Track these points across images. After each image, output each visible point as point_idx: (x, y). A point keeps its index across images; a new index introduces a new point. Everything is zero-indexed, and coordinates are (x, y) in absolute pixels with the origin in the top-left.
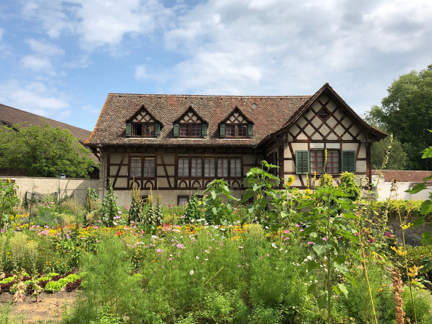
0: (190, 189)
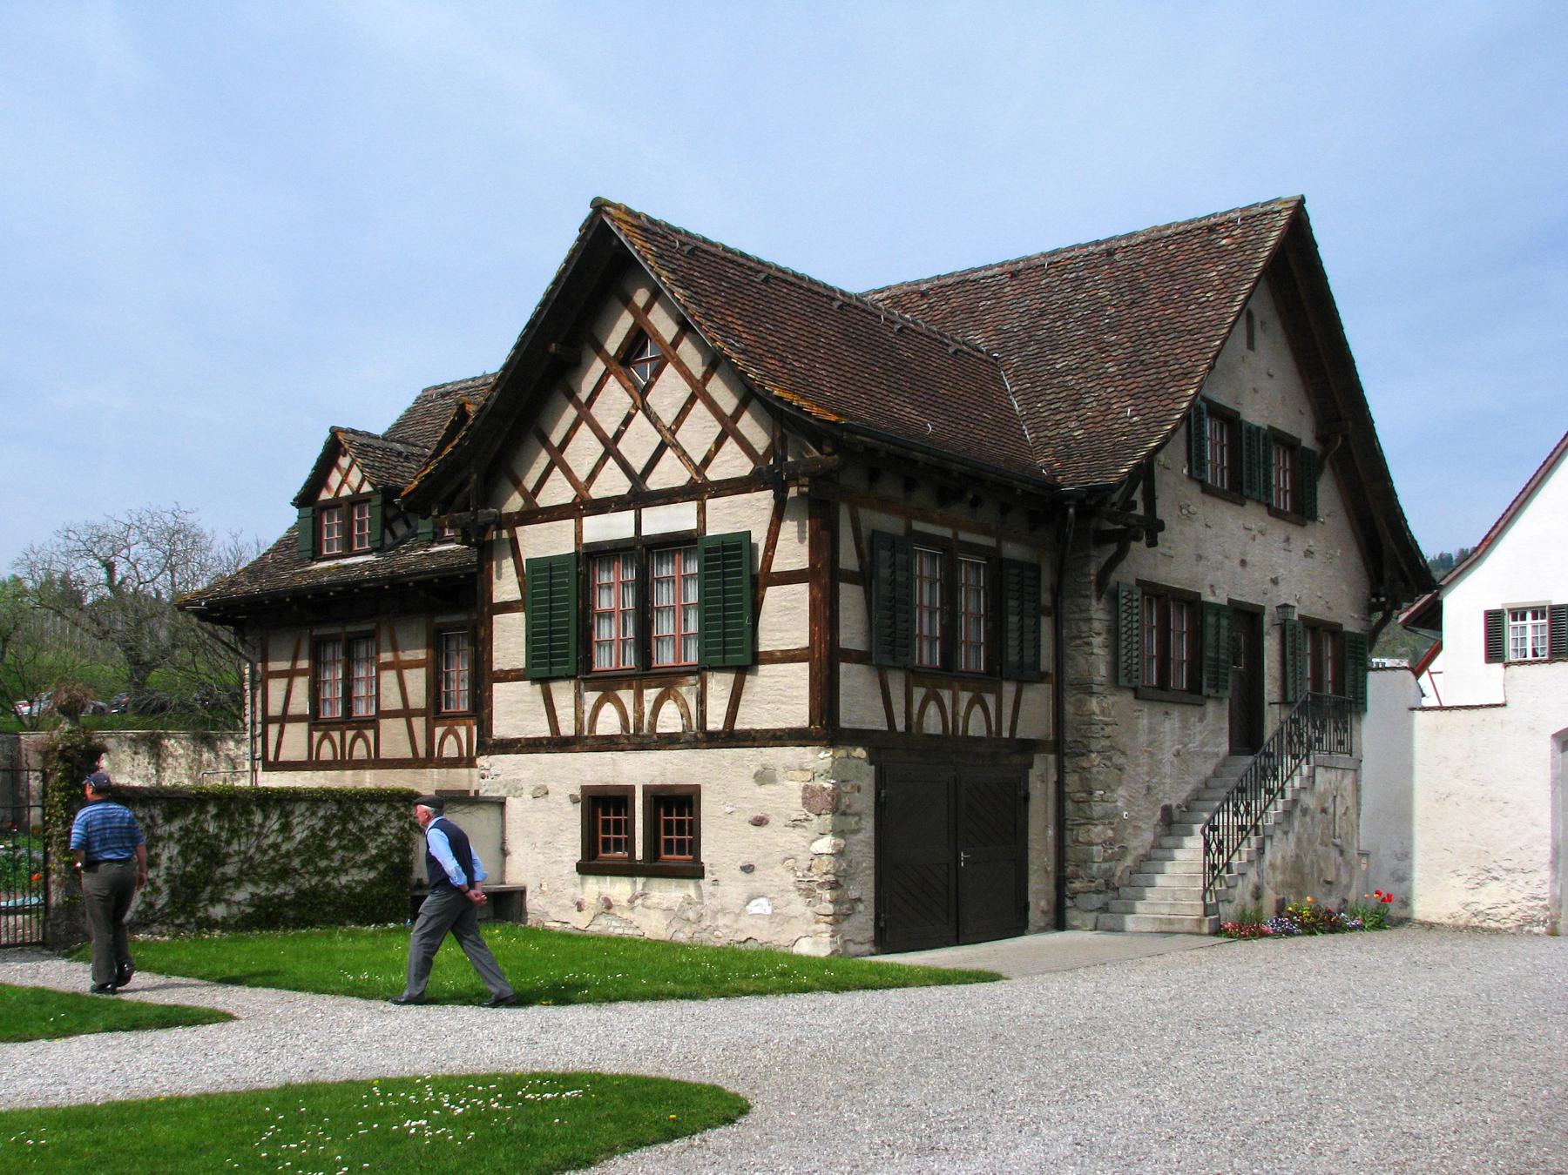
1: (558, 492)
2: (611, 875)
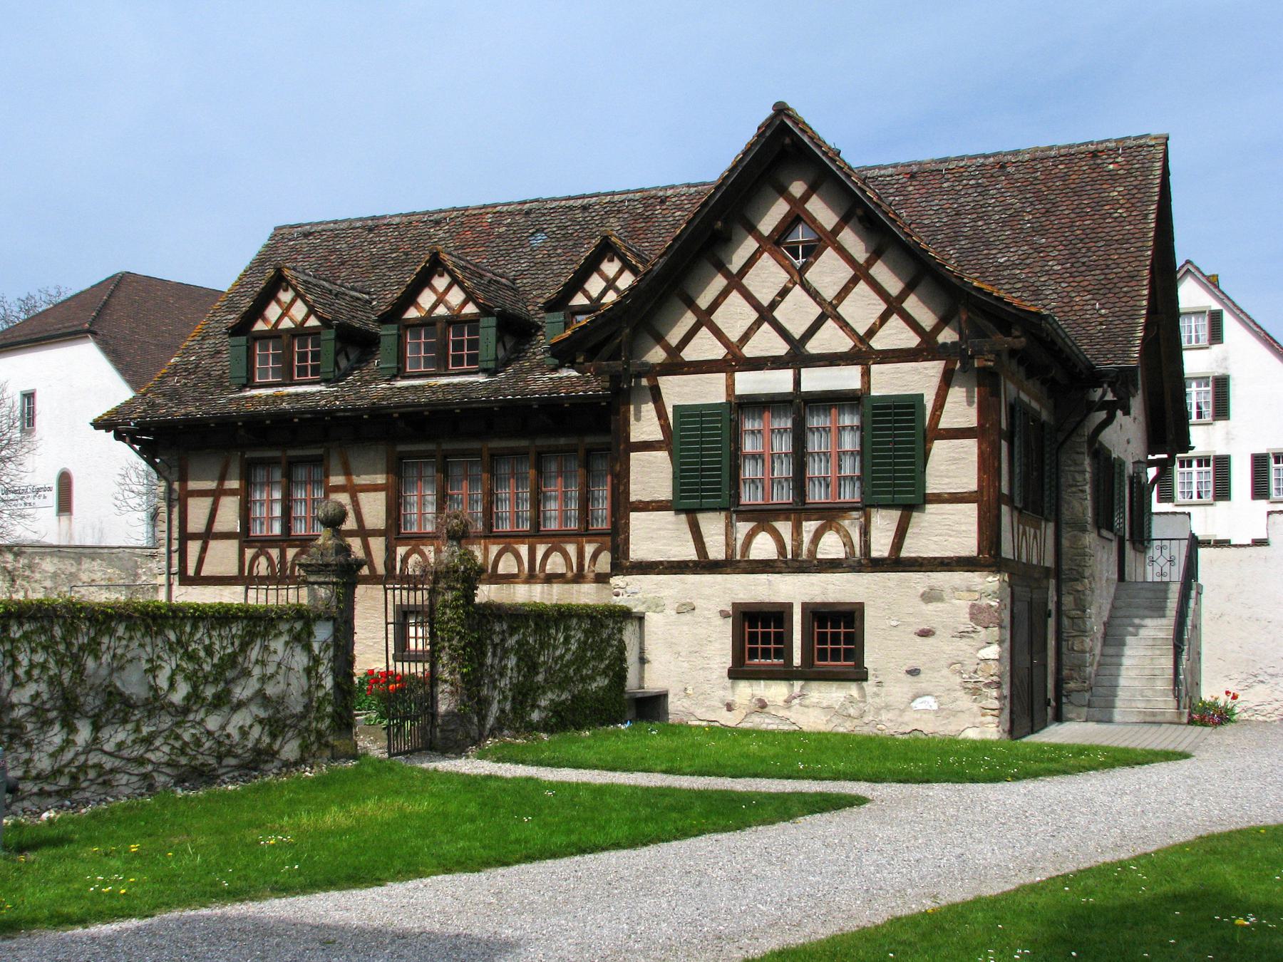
0: (531, 578)
1: (705, 347)
2: (764, 679)
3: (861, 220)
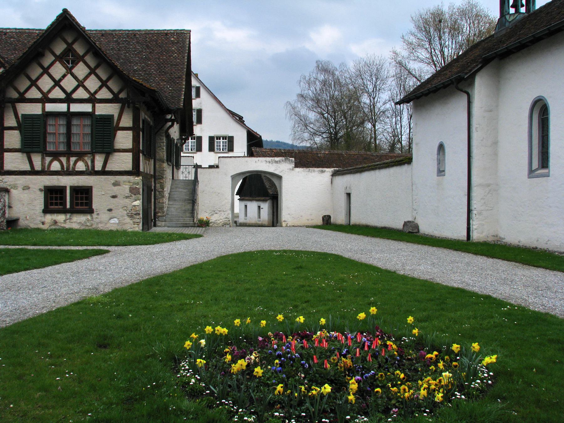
3: (93, 53)
